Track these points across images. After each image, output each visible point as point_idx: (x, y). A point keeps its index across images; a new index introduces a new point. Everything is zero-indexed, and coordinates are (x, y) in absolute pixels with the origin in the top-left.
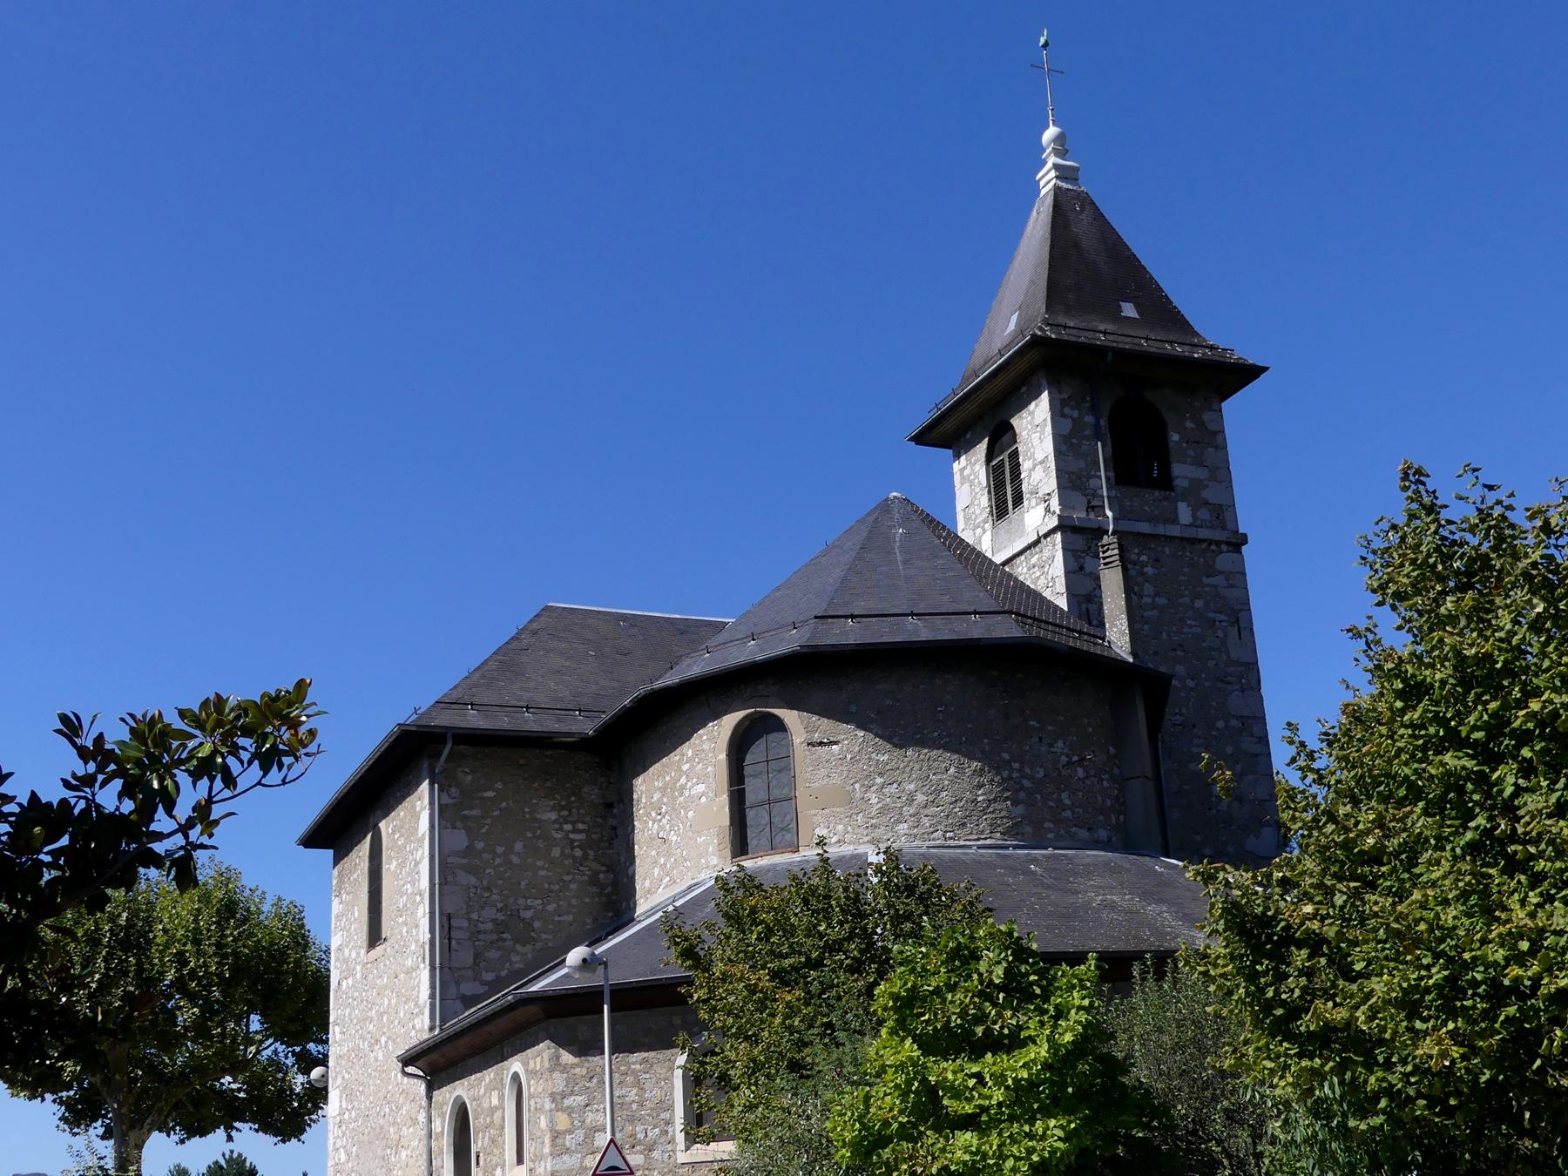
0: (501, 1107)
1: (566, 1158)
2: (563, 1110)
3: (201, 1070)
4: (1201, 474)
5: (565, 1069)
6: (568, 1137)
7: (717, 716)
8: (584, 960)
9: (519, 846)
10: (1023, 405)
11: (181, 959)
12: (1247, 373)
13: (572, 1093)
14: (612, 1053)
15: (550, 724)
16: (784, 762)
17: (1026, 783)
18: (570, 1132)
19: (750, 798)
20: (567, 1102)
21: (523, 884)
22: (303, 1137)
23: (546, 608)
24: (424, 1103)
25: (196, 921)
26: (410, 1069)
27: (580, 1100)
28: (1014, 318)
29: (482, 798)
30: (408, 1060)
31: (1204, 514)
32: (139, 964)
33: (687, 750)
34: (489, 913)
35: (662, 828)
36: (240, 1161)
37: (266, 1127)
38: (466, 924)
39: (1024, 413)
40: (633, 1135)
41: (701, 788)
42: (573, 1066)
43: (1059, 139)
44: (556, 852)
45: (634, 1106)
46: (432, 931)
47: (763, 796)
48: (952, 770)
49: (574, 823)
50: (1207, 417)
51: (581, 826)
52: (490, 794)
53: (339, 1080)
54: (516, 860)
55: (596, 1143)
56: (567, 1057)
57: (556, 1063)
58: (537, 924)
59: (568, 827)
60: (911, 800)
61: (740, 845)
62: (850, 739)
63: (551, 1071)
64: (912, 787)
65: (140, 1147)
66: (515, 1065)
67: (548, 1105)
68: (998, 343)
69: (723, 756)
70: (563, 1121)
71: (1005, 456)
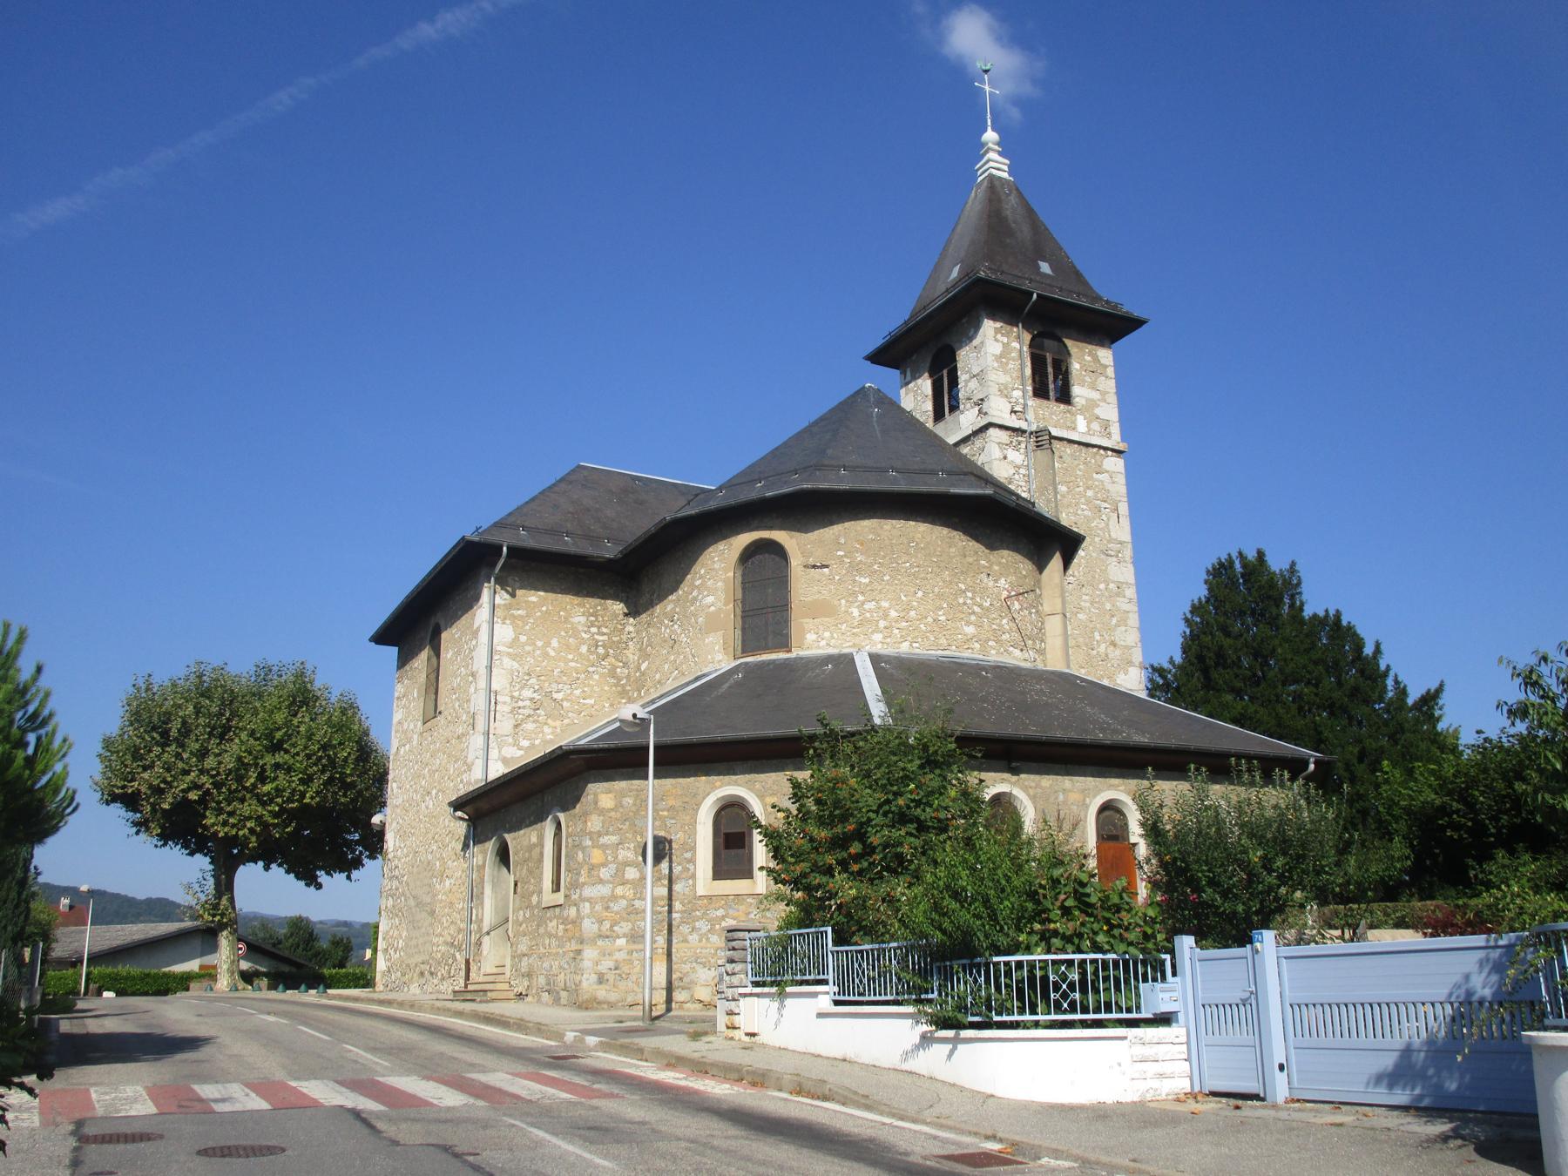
0: (541, 844)
2: (599, 847)
4: (1095, 395)
9: (555, 643)
12: (1137, 323)
15: (587, 549)
17: (976, 609)
18: (604, 865)
22: (355, 874)
23: (579, 467)
26: (459, 814)
27: (614, 839)
28: (957, 269)
30: (457, 805)
31: (1096, 426)
34: (527, 693)
35: (674, 632)
38: (508, 699)
44: (584, 649)
54: (552, 653)
58: (565, 704)
59: (594, 630)
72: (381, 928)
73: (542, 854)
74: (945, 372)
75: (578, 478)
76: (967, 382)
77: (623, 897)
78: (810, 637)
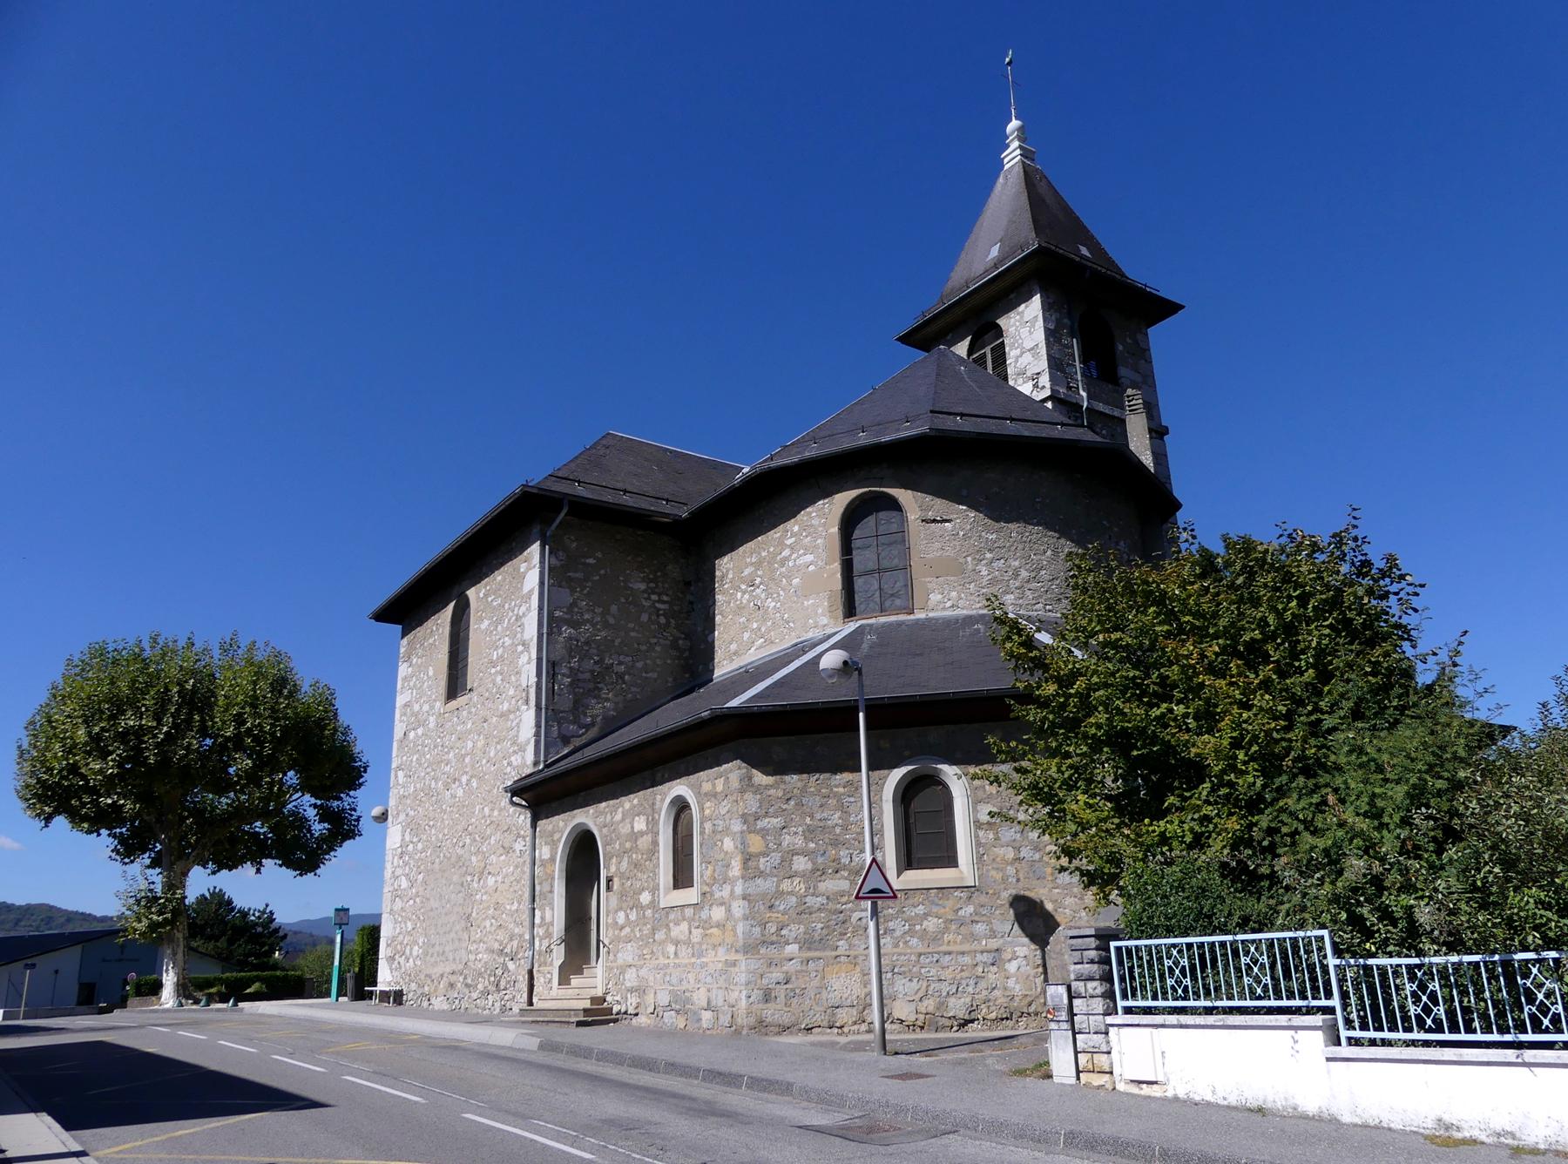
1: (759, 881)
3: (240, 814)
5: (758, 789)
6: (762, 860)
7: (828, 494)
8: (845, 663)
9: (614, 608)
10: (1013, 306)
11: (239, 720)
12: (1168, 308)
13: (767, 815)
14: (872, 767)
16: (900, 538)
18: (765, 854)
19: (858, 567)
20: (760, 824)
21: (617, 642)
24: (529, 832)
25: (254, 690)
27: (776, 822)
29: (585, 564)
32: (203, 721)
33: (793, 526)
36: (221, 894)
37: (288, 863)
39: (1012, 314)
40: (836, 860)
41: (810, 558)
42: (767, 787)
43: (1020, 129)
44: (644, 618)
45: (838, 830)
46: (539, 675)
47: (872, 565)
48: (1049, 553)
49: (659, 595)
50: (1139, 337)
51: (665, 598)
52: (591, 561)
53: (402, 817)
54: (611, 621)
55: (795, 867)
56: (760, 778)
57: (747, 781)
59: (654, 597)
60: (1016, 575)
61: (850, 611)
62: (963, 518)
63: (742, 791)
64: (1017, 563)
65: (185, 874)
66: (679, 788)
67: (737, 826)
68: (979, 268)
69: (835, 530)
70: (756, 843)
71: (988, 350)
72: (383, 933)
73: (655, 843)
74: (988, 350)
75: (607, 443)
76: (1017, 358)
77: (791, 893)
78: (935, 598)
